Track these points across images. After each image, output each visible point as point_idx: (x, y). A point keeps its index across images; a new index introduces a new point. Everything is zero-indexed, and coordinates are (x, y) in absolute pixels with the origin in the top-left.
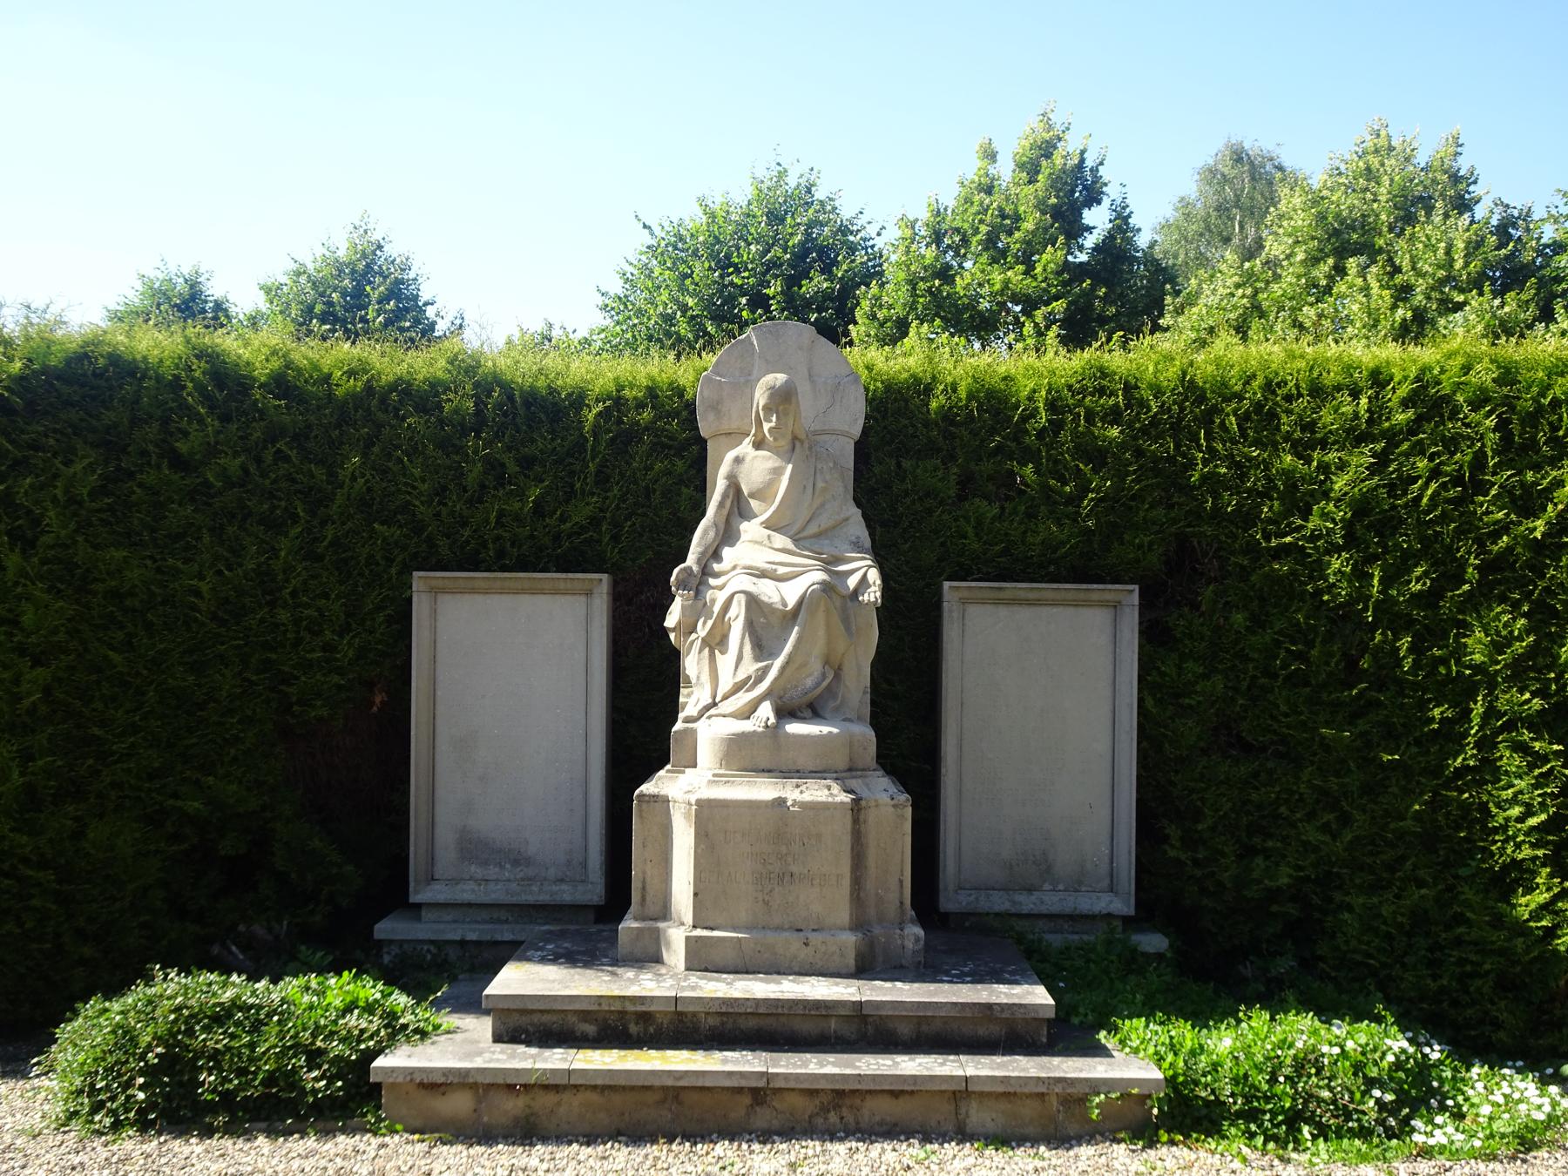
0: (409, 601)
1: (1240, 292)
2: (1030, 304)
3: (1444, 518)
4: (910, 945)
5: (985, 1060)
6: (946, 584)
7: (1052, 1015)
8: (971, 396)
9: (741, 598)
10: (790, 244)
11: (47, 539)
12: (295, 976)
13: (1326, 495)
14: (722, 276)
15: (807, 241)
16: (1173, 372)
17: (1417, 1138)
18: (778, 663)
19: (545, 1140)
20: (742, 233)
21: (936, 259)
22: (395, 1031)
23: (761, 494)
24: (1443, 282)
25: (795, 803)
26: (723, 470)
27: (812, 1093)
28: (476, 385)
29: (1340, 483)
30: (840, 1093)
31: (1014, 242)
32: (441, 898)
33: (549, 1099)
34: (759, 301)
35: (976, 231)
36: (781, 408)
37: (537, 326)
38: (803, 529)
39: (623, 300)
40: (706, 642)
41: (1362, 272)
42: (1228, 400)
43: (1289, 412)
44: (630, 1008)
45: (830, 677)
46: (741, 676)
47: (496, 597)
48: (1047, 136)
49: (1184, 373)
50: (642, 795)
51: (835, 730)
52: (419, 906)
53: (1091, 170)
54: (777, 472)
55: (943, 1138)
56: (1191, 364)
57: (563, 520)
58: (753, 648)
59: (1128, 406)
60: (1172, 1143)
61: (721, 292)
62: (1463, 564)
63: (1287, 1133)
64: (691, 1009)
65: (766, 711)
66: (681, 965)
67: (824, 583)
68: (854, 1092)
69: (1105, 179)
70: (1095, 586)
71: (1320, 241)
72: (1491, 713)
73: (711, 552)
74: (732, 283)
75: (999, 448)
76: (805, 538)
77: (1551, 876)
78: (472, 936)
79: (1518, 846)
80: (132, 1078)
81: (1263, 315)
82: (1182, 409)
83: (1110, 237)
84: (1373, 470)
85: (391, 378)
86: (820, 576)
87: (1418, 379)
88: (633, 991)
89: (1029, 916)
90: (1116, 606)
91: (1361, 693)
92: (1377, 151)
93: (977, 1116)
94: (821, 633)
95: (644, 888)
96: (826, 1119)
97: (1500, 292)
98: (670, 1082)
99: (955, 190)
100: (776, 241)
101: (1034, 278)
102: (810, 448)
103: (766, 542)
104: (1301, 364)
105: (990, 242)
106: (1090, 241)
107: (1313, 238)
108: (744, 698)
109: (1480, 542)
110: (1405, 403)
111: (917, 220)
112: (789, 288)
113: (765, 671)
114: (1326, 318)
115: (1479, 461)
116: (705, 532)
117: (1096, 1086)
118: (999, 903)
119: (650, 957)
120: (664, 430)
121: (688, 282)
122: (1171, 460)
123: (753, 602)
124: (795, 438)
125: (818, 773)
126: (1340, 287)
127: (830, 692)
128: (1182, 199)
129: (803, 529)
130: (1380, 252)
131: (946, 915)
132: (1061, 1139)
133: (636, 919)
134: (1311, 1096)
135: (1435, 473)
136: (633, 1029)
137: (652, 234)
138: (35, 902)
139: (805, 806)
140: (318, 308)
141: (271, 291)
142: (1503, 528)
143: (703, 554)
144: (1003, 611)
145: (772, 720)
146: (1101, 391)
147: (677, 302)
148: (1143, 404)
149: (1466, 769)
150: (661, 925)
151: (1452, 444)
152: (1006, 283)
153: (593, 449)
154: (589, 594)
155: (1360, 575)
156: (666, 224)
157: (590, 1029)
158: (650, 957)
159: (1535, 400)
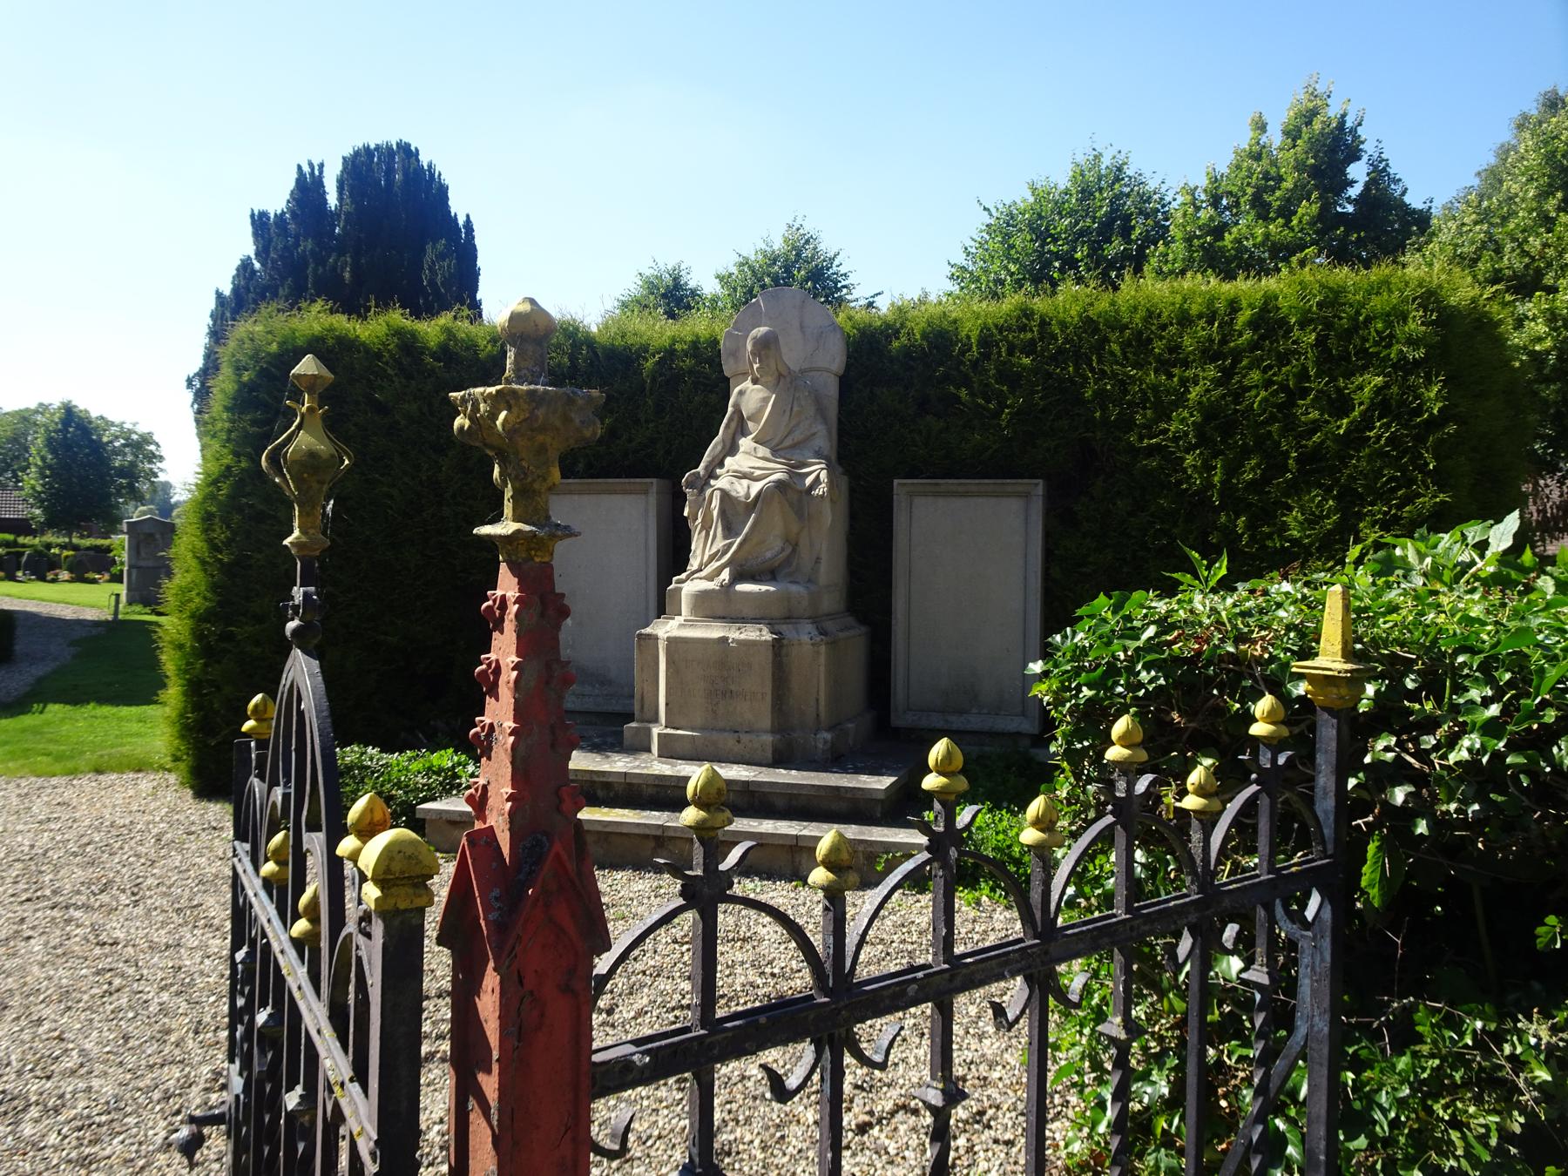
1: (1478, 227)
3: (1272, 419)
6: (896, 482)
8: (924, 336)
10: (1098, 214)
14: (1042, 246)
15: (1112, 211)
18: (738, 540)
23: (755, 417)
29: (1195, 393)
31: (1274, 199)
34: (1069, 263)
38: (781, 442)
42: (1113, 329)
44: (596, 778)
46: (714, 550)
48: (1311, 105)
50: (641, 634)
51: (772, 589)
53: (1350, 132)
54: (765, 400)
57: (630, 440)
59: (1041, 339)
62: (1286, 455)
71: (1549, 177)
73: (717, 461)
74: (1050, 251)
82: (1080, 339)
83: (1367, 186)
84: (1218, 383)
90: (1026, 496)
98: (600, 828)
99: (1230, 158)
101: (1292, 229)
106: (1354, 192)
107: (1544, 175)
108: (715, 564)
110: (1253, 324)
111: (1196, 188)
113: (729, 546)
114: (1549, 246)
115: (1303, 375)
121: (1013, 252)
122: (1071, 380)
123: (725, 495)
124: (780, 375)
125: (755, 620)
127: (788, 561)
128: (1503, 146)
129: (781, 442)
131: (897, 730)
135: (1268, 384)
136: (600, 793)
137: (991, 215)
139: (739, 642)
141: (723, 279)
142: (1315, 427)
143: (710, 463)
144: (941, 502)
146: (1023, 328)
148: (1054, 337)
151: (1283, 359)
152: (1267, 236)
155: (1208, 468)
156: (1000, 206)
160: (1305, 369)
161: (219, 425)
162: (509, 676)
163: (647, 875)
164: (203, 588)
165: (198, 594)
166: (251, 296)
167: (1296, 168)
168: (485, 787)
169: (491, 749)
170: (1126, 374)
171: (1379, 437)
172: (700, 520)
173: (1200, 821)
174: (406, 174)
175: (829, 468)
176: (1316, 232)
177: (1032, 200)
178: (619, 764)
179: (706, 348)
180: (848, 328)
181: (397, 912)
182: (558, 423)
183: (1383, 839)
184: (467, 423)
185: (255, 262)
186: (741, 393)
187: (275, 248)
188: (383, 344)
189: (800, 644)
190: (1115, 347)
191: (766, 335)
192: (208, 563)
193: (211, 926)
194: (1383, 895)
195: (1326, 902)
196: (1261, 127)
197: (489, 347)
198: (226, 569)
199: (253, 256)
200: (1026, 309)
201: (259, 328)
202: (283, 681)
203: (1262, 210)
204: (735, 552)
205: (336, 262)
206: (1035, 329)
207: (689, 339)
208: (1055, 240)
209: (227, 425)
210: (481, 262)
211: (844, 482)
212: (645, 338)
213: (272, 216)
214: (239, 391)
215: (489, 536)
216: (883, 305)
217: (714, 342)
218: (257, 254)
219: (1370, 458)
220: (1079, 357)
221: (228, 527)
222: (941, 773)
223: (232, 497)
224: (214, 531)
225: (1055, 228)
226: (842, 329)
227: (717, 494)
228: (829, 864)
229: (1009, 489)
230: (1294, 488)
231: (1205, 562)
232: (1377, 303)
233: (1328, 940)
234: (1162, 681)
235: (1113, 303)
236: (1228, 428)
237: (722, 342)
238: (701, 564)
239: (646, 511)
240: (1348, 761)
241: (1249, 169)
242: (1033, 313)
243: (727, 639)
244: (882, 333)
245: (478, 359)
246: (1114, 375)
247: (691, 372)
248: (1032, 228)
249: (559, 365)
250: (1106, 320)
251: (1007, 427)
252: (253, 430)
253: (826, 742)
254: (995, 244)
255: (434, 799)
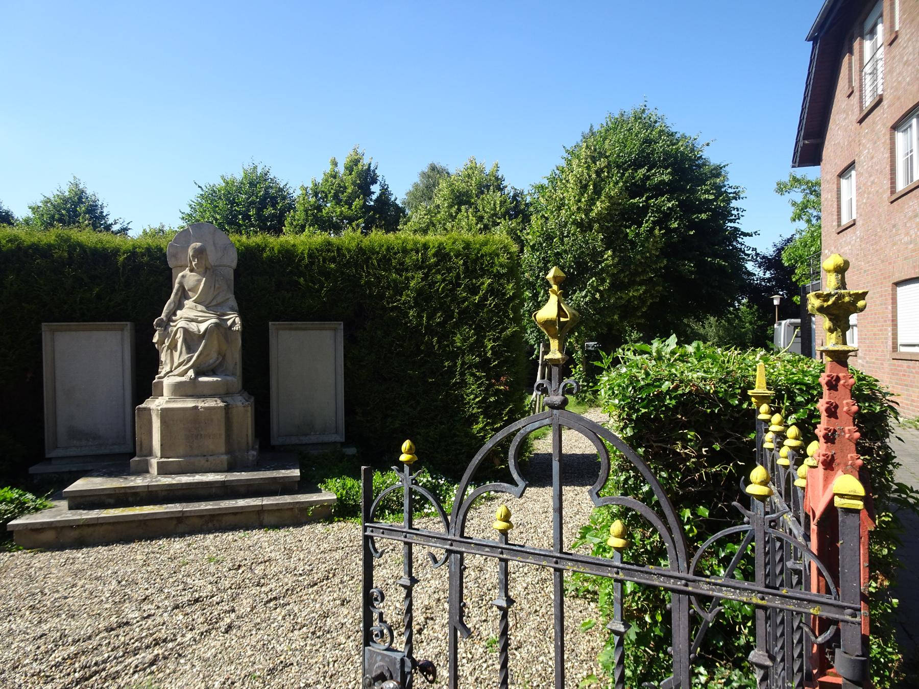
0: (41, 335)
2: (351, 220)
3: (447, 296)
4: (251, 458)
5: (272, 498)
6: (270, 323)
7: (299, 479)
8: (279, 252)
9: (182, 330)
12: (339, 477)
13: (408, 288)
14: (231, 207)
16: (354, 244)
17: (426, 510)
18: (196, 354)
19: (87, 546)
20: (239, 190)
21: (315, 202)
22: (22, 509)
23: (194, 289)
24: (493, 215)
25: (202, 407)
26: (177, 281)
27: (201, 517)
28: (69, 246)
29: (412, 284)
31: (343, 197)
32: (60, 455)
33: (90, 530)
35: (330, 192)
37: (157, 226)
39: (190, 215)
40: (169, 348)
41: (467, 211)
42: (373, 254)
43: (395, 259)
44: (129, 491)
45: (220, 359)
46: (181, 360)
47: (82, 332)
48: (356, 157)
49: (359, 244)
50: (139, 408)
51: (219, 379)
52: (50, 459)
55: (252, 528)
56: (361, 241)
59: (338, 256)
60: (339, 521)
61: (231, 213)
62: (453, 311)
63: (380, 514)
64: (154, 489)
65: (191, 373)
66: (156, 473)
67: (216, 323)
68: (218, 515)
69: (378, 174)
72: (463, 363)
74: (235, 210)
75: (291, 272)
77: (484, 418)
78: (75, 469)
79: (473, 408)
81: (434, 226)
82: (358, 257)
83: (381, 195)
84: (423, 279)
85: (29, 243)
86: (214, 320)
87: (439, 247)
88: (132, 484)
89: (306, 444)
90: (335, 330)
91: (422, 358)
92: (471, 168)
93: (267, 519)
94: (216, 342)
95: (141, 444)
97: (510, 219)
98: (141, 518)
100: (253, 194)
101: (352, 210)
104: (400, 241)
105: (336, 197)
106: (374, 197)
108: (183, 368)
109: (458, 304)
110: (435, 255)
112: (259, 212)
113: (191, 358)
115: (458, 277)
116: (170, 304)
117: (311, 503)
118: (294, 440)
119: (143, 470)
121: (217, 209)
122: (354, 276)
123: (186, 331)
126: (459, 216)
127: (221, 364)
130: (473, 204)
132: (298, 524)
133: (138, 457)
134: (390, 500)
135: (444, 280)
136: (131, 499)
139: (205, 408)
140: (57, 216)
141: (34, 209)
142: (465, 299)
143: (168, 313)
144: (293, 333)
145: (193, 376)
146: (329, 251)
147: (213, 216)
148: (344, 255)
149: (456, 383)
150: (148, 458)
151: (449, 270)
152: (342, 212)
154: (122, 330)
156: (208, 186)
157: (112, 501)
158: (143, 470)
159: (476, 255)
160: (458, 274)
167: (352, 184)
171: (490, 304)
176: (363, 213)
178: (138, 482)
189: (237, 407)
196: (335, 164)
203: (338, 201)
208: (238, 205)
216: (135, 233)
219: (487, 313)
220: (356, 265)
229: (327, 326)
230: (458, 325)
232: (485, 249)
236: (428, 299)
239: (122, 339)
241: (332, 182)
243: (197, 407)
249: (60, 257)
253: (254, 456)
255: (14, 518)
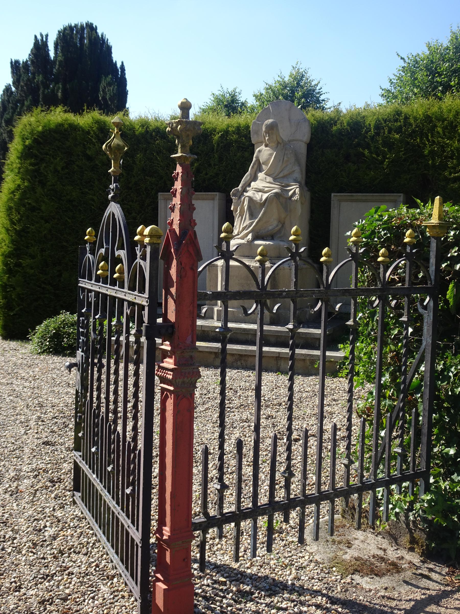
6: (333, 194)
8: (349, 124)
11: (49, 183)
14: (433, 78)
18: (256, 220)
23: (266, 163)
30: (241, 356)
36: (270, 132)
38: (278, 175)
42: (439, 120)
45: (280, 226)
46: (245, 225)
51: (271, 243)
54: (271, 155)
58: (249, 216)
59: (405, 126)
64: (206, 329)
68: (245, 355)
70: (386, 194)
73: (247, 184)
74: (437, 82)
76: (278, 178)
80: (47, 339)
82: (423, 126)
96: (237, 363)
102: (283, 146)
103: (264, 180)
108: (245, 232)
113: (252, 223)
120: (242, 142)
121: (416, 82)
123: (251, 199)
124: (278, 143)
127: (279, 231)
138: (47, 295)
141: (258, 97)
143: (244, 184)
146: (396, 120)
148: (411, 125)
153: (217, 150)
161: (15, 165)
162: (179, 191)
163: (211, 369)
164: (7, 242)
165: (5, 245)
166: (10, 105)
168: (173, 220)
169: (174, 210)
170: (444, 142)
172: (238, 212)
173: (383, 265)
174: (90, 40)
175: (300, 187)
177: (428, 52)
179: (243, 130)
180: (312, 120)
181: (154, 243)
182: (192, 129)
183: (455, 283)
184: (170, 129)
185: (12, 87)
186: (260, 151)
187: (23, 80)
188: (91, 127)
190: (439, 129)
191: (272, 123)
192: (10, 230)
193: (24, 379)
194: (454, 301)
195: (431, 299)
197: (140, 129)
198: (18, 233)
199: (11, 84)
200: (398, 111)
201: (33, 119)
202: (106, 213)
204: (255, 226)
205: (54, 87)
206: (402, 121)
207: (235, 125)
208: (440, 75)
209: (19, 165)
210: (129, 87)
211: (308, 195)
212: (215, 125)
213: (21, 62)
214: (24, 149)
215: (175, 157)
217: (247, 127)
218: (14, 83)
220: (422, 134)
221: (19, 213)
222: (294, 235)
223: (20, 199)
224: (13, 215)
225: (440, 69)
226: (309, 121)
227: (247, 199)
228: (261, 254)
231: (422, 204)
233: (432, 312)
234: (389, 235)
235: (440, 108)
237: (251, 127)
238: (238, 232)
240: (441, 258)
242: (401, 113)
244: (328, 122)
245: (135, 135)
246: (439, 143)
247: (236, 141)
248: (427, 68)
250: (435, 116)
251: (386, 168)
252: (30, 168)
254: (407, 77)
